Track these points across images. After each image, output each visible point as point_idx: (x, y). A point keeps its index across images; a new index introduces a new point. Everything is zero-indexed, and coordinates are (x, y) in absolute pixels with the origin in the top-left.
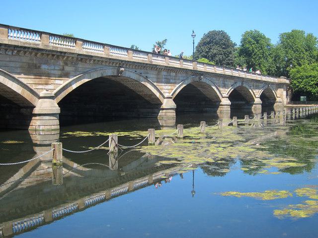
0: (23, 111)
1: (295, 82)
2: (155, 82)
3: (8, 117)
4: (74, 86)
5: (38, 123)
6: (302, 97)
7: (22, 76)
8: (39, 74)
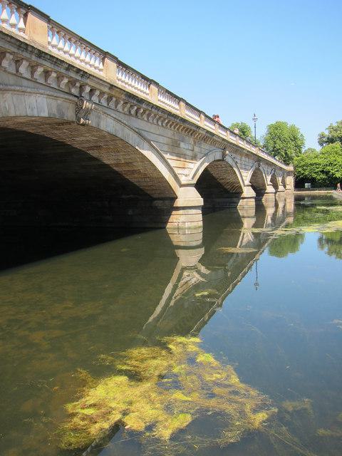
0: (158, 204)
1: (300, 169)
2: (166, 152)
3: (130, 212)
5: (182, 219)
6: (306, 184)
8: (180, 155)
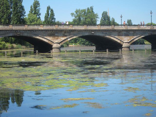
4: (137, 39)
7: (48, 37)
